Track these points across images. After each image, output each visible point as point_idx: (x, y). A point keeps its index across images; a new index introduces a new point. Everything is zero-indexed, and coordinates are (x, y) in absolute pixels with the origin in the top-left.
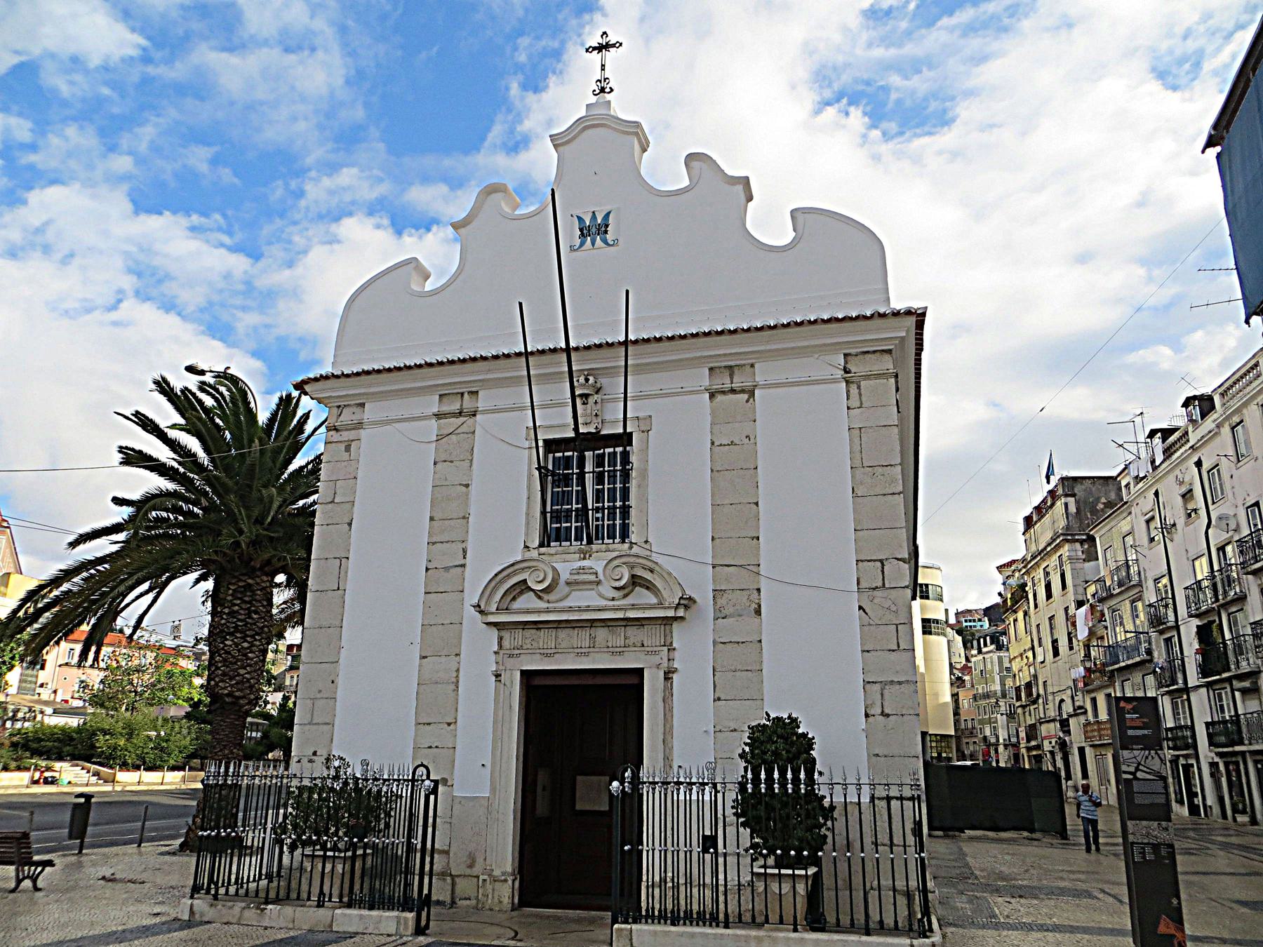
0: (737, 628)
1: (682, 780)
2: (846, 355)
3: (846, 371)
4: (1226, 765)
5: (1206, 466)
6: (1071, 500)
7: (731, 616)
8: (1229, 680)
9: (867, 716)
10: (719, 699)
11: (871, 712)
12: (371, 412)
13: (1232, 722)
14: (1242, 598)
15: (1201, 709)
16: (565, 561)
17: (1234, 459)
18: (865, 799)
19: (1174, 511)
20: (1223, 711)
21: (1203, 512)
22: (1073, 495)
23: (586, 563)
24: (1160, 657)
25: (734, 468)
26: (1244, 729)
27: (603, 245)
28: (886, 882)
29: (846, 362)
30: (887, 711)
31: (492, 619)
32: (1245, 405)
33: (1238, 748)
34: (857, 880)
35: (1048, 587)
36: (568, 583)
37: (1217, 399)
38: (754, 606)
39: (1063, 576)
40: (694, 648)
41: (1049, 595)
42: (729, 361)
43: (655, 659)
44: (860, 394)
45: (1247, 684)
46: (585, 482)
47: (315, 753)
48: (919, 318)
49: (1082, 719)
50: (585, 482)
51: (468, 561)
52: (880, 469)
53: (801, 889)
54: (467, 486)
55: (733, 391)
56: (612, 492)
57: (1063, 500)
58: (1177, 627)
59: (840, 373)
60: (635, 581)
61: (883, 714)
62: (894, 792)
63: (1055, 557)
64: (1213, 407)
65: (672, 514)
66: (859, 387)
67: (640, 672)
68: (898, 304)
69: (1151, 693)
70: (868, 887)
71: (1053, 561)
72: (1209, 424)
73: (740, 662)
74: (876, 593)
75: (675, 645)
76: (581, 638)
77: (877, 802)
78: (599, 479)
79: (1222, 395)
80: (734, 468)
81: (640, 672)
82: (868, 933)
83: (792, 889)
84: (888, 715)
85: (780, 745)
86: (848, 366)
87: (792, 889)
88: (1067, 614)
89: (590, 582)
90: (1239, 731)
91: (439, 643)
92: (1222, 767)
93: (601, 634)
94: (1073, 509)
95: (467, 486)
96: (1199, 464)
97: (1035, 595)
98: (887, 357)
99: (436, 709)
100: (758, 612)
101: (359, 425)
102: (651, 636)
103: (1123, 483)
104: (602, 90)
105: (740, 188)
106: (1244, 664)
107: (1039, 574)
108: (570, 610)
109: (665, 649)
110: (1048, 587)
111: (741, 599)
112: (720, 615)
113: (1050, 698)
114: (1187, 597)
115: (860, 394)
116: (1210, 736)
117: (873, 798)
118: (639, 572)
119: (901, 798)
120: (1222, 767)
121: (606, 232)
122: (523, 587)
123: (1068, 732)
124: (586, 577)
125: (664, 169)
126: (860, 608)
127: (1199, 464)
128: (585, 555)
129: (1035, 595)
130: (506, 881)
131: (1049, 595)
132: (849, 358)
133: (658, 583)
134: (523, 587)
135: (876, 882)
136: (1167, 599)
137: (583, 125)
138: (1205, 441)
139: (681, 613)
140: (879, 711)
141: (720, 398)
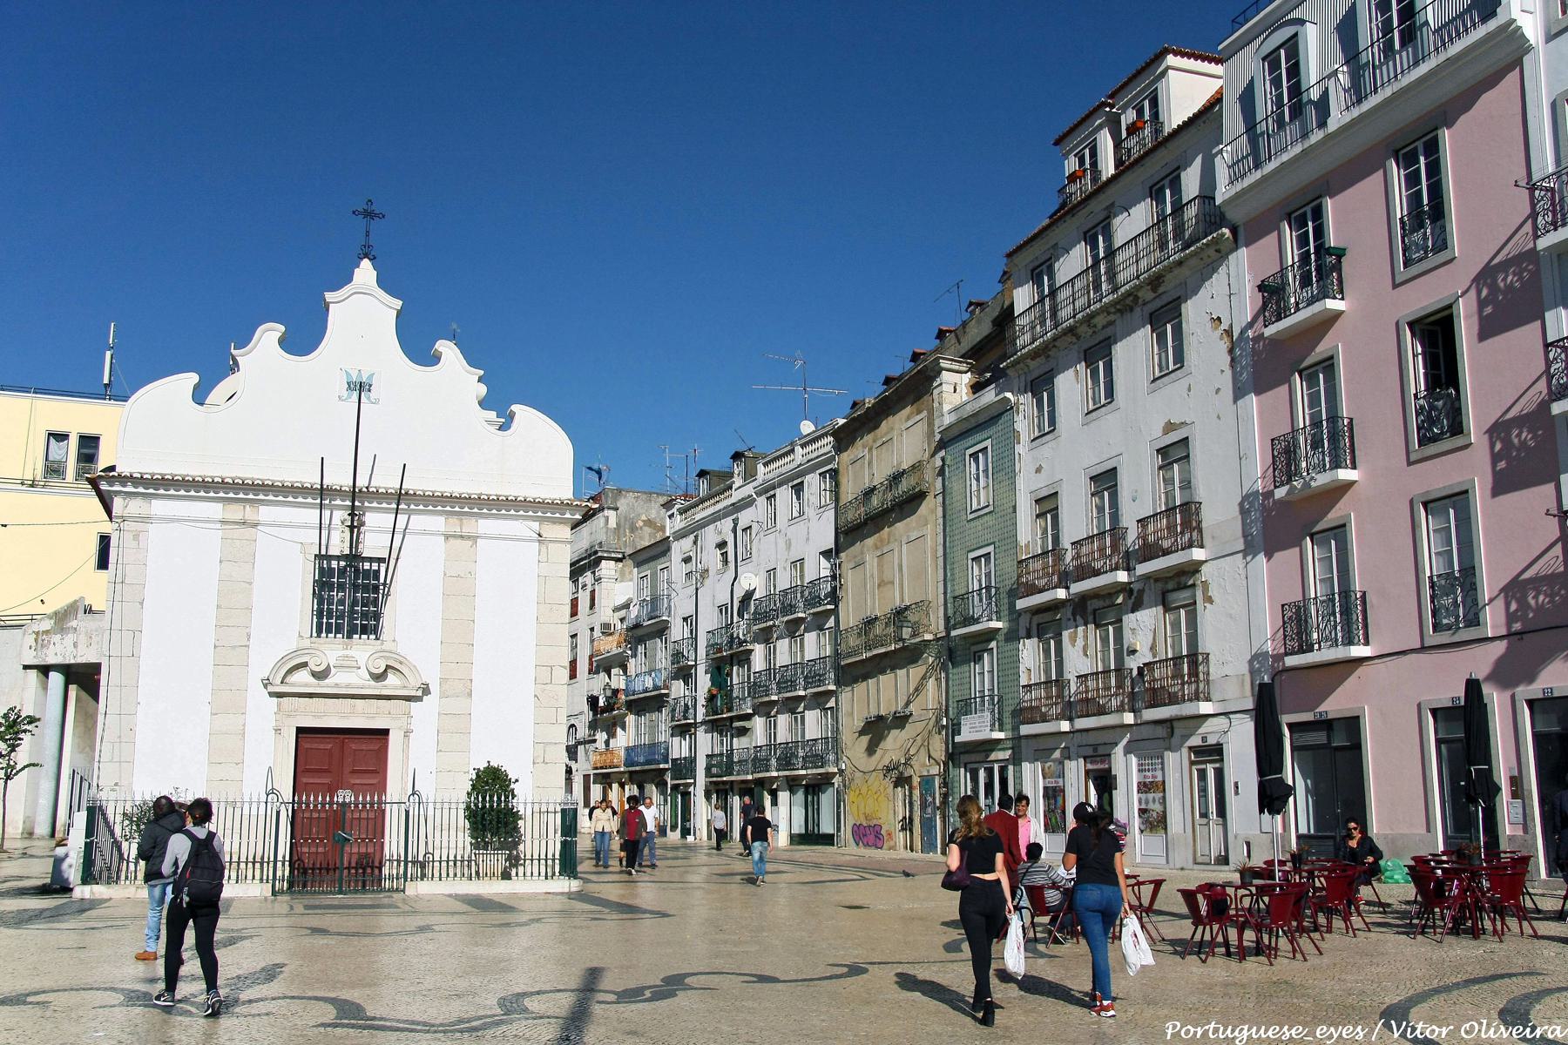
16: (332, 650)
25: (459, 589)
46: (350, 595)
50: (350, 595)
73: (456, 727)
85: (492, 781)
94: (613, 524)
100: (470, 695)
112: (443, 695)
116: (1279, 319)
124: (353, 660)
141: (452, 540)
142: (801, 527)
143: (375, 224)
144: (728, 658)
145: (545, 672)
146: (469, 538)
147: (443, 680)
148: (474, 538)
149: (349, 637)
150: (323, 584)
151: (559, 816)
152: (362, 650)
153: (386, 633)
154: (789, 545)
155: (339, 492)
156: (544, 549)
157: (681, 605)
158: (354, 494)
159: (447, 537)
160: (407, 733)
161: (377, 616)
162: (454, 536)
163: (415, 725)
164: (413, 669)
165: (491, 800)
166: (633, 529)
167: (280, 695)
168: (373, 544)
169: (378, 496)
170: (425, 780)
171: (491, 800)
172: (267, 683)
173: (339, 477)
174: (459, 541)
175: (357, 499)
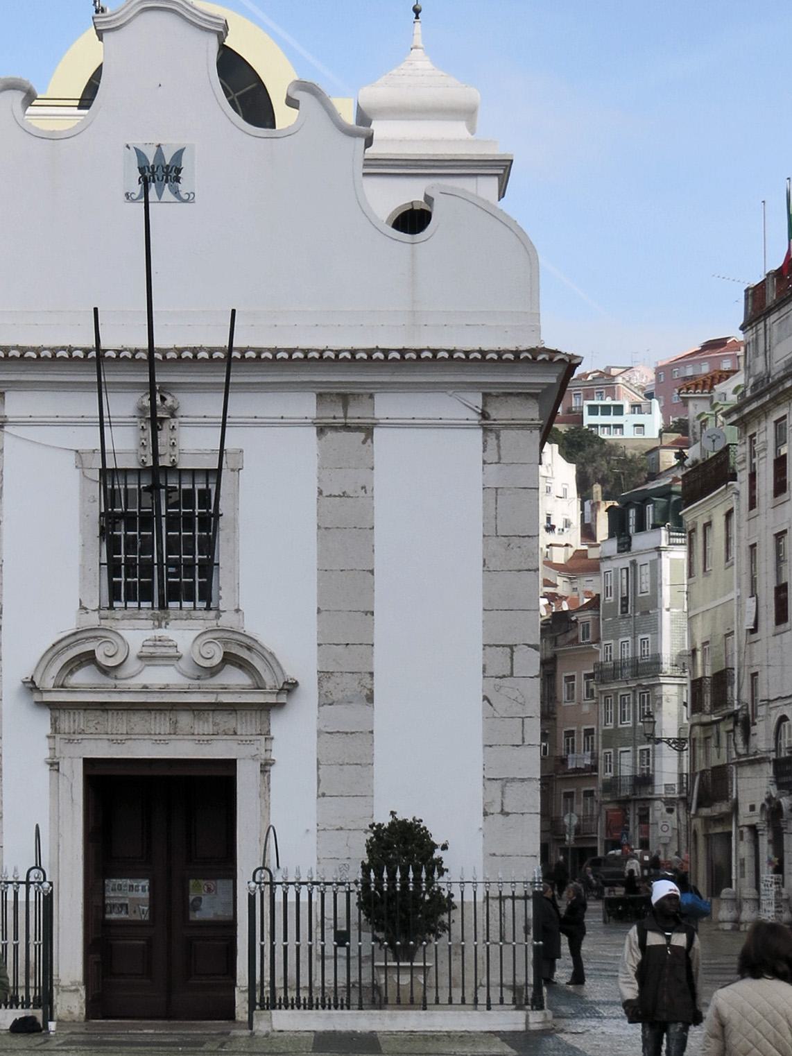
0: (346, 717)
1: (32, 879)
3: (484, 415)
7: (339, 702)
9: (485, 814)
10: (324, 795)
16: (135, 631)
18: (480, 899)
25: (345, 526)
27: (173, 198)
28: (495, 979)
29: (485, 404)
30: (507, 809)
31: (48, 698)
34: (470, 976)
36: (140, 658)
38: (366, 692)
40: (295, 737)
43: (250, 750)
44: (499, 447)
46: (159, 536)
50: (159, 536)
52: (516, 540)
55: (346, 427)
59: (475, 417)
62: (507, 891)
65: (268, 573)
66: (498, 438)
67: (233, 763)
70: (478, 984)
73: (347, 753)
75: (272, 734)
76: (160, 724)
77: (490, 901)
80: (345, 526)
81: (233, 763)
84: (507, 814)
85: (402, 846)
86: (488, 410)
93: (185, 719)
97: (753, 477)
100: (370, 699)
102: (246, 725)
108: (145, 689)
109: (263, 738)
112: (326, 700)
113: (762, 711)
115: (499, 447)
117: (487, 898)
118: (235, 650)
121: (177, 180)
122: (88, 658)
124: (160, 649)
126: (485, 698)
128: (160, 622)
129: (753, 477)
130: (77, 990)
132: (489, 399)
134: (88, 658)
135: (485, 979)
140: (499, 810)
141: (330, 435)
144: (257, 883)
145: (501, 655)
146: (358, 428)
148: (368, 430)
150: (111, 524)
151: (530, 903)
152: (185, 632)
155: (124, 360)
156: (492, 436)
158: (152, 360)
159: (321, 430)
160: (266, 767)
161: (208, 568)
162: (334, 428)
163: (278, 752)
164: (270, 659)
165: (392, 878)
167: (53, 706)
168: (192, 444)
169: (188, 360)
170: (294, 834)
171: (392, 878)
173: (125, 335)
174: (343, 435)
175: (155, 375)
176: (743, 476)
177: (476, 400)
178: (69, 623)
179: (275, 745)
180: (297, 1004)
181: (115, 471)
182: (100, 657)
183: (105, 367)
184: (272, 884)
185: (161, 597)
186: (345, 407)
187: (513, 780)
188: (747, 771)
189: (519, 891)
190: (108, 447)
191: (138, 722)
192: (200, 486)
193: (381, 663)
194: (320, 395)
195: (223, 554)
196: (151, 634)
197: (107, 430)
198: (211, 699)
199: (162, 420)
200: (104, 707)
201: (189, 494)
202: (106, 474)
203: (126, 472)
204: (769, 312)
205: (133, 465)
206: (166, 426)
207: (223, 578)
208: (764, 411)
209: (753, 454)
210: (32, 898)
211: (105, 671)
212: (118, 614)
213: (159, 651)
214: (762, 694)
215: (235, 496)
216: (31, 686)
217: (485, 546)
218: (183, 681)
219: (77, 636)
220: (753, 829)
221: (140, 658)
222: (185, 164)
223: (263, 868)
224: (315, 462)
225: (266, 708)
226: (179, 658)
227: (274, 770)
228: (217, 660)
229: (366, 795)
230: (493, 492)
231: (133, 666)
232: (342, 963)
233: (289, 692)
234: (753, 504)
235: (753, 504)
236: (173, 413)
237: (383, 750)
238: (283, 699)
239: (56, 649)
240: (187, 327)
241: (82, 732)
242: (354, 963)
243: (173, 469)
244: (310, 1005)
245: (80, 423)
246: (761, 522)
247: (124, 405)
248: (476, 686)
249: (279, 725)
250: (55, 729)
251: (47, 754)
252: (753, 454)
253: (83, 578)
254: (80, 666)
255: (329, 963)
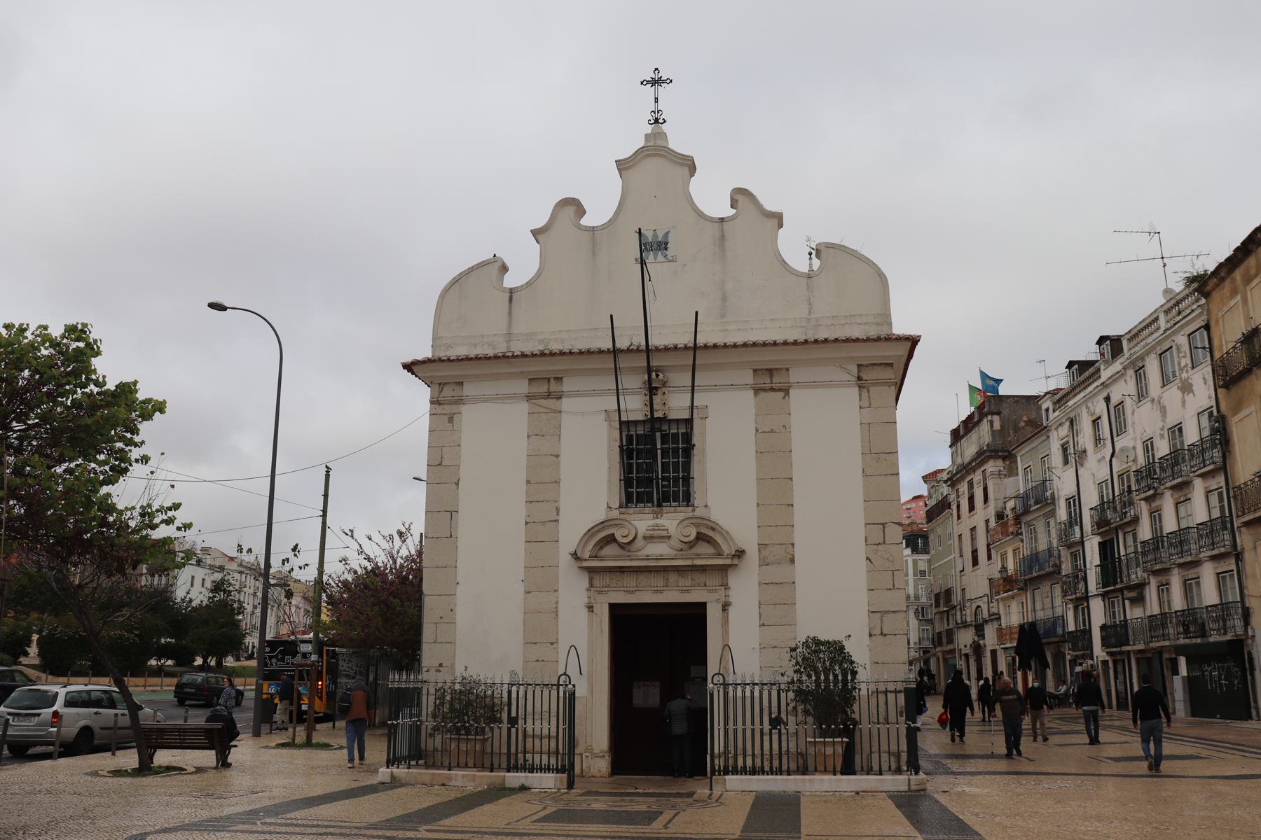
2: (859, 366)
3: (859, 378)
4: (1115, 662)
5: (1114, 401)
6: (996, 418)
7: (773, 564)
8: (1121, 590)
9: (870, 635)
11: (873, 632)
12: (469, 390)
13: (1121, 626)
14: (1136, 520)
15: (1098, 613)
16: (642, 521)
17: (1135, 398)
19: (1086, 438)
20: (1114, 617)
21: (1109, 442)
22: (998, 413)
23: (658, 521)
24: (1066, 568)
25: (774, 453)
26: (1130, 633)
28: (884, 747)
31: (585, 564)
32: (1148, 353)
33: (1125, 648)
35: (971, 499)
37: (1125, 343)
39: (985, 489)
40: (745, 589)
41: (972, 508)
42: (770, 369)
43: (715, 596)
45: (1133, 594)
46: (656, 462)
47: (441, 665)
48: (914, 341)
49: (996, 625)
50: (656, 462)
51: (561, 518)
53: (840, 750)
54: (557, 456)
55: (772, 389)
56: (676, 465)
57: (989, 417)
58: (1082, 543)
60: (700, 537)
61: (882, 634)
63: (979, 472)
64: (1122, 350)
68: (899, 329)
69: (1059, 612)
71: (977, 477)
72: (1117, 366)
73: (779, 597)
74: (880, 547)
76: (658, 581)
78: (665, 453)
79: (1129, 340)
80: (774, 453)
81: (703, 605)
82: (881, 774)
83: (834, 748)
87: (834, 748)
88: (987, 526)
89: (663, 537)
90: (1127, 634)
91: (539, 582)
92: (1111, 665)
93: (673, 577)
94: (997, 426)
95: (557, 456)
96: (1108, 399)
97: (958, 507)
98: (889, 369)
99: (540, 627)
100: (792, 561)
101: (459, 401)
102: (713, 581)
103: (1044, 407)
104: (657, 121)
105: (776, 221)
106: (1133, 577)
107: (964, 487)
108: (648, 558)
110: (971, 499)
111: (780, 552)
112: (764, 563)
113: (968, 604)
114: (1092, 517)
116: (1103, 639)
119: (896, 692)
120: (1111, 665)
123: (982, 636)
124: (658, 531)
125: (710, 195)
126: (868, 558)
127: (1108, 399)
128: (657, 515)
129: (958, 507)
131: (972, 508)
133: (719, 539)
134: (611, 539)
136: (1075, 519)
137: (641, 154)
138: (1115, 378)
139: (736, 561)
141: (762, 394)
142: (1171, 421)
143: (663, 90)
144: (1112, 523)
145: (876, 533)
146: (780, 390)
147: (762, 546)
148: (786, 391)
149: (659, 505)
151: (901, 697)
152: (672, 521)
153: (697, 499)
154: (1163, 411)
157: (1063, 484)
159: (757, 391)
160: (725, 607)
161: (687, 480)
162: (765, 390)
164: (726, 535)
166: (1016, 429)
167: (591, 570)
168: (676, 404)
170: (744, 649)
172: (575, 555)
173: (630, 336)
175: (650, 363)
176: (954, 507)
177: (854, 370)
178: (601, 515)
179: (731, 593)
180: (744, 771)
181: (628, 422)
182: (618, 537)
183: (621, 357)
184: (725, 685)
185: (658, 499)
186: (771, 377)
187: (888, 612)
188: (962, 631)
189: (900, 687)
190: (622, 407)
191: (643, 579)
192: (682, 430)
193: (799, 536)
194: (755, 371)
195: (696, 470)
196: (652, 522)
197: (621, 398)
198: (689, 562)
199: (657, 388)
200: (622, 570)
201: (676, 435)
202: (625, 425)
203: (636, 422)
204: (962, 437)
205: (641, 417)
206: (660, 392)
207: (696, 486)
208: (962, 478)
209: (958, 496)
210: (561, 694)
211: (622, 546)
212: (631, 510)
213: (656, 533)
214: (968, 597)
215: (703, 434)
216: (575, 555)
217: (864, 460)
218: (673, 553)
219: (603, 524)
220: (967, 655)
221: (645, 538)
222: (670, 239)
223: (565, 674)
224: (753, 411)
225: (724, 569)
226: (669, 537)
227: (731, 609)
228: (693, 537)
229: (792, 624)
230: (867, 426)
231: (640, 542)
232: (775, 737)
233: (739, 557)
234: (959, 517)
235: (959, 517)
236: (664, 384)
237: (802, 594)
238: (736, 561)
239: (591, 532)
240: (670, 330)
241: (608, 586)
242: (784, 738)
243: (664, 419)
244: (753, 772)
245: (602, 393)
246: (963, 524)
247: (634, 382)
248: (861, 551)
249: (733, 579)
250: (591, 585)
251: (586, 600)
252: (958, 496)
253: (609, 489)
254: (608, 543)
255: (766, 738)
